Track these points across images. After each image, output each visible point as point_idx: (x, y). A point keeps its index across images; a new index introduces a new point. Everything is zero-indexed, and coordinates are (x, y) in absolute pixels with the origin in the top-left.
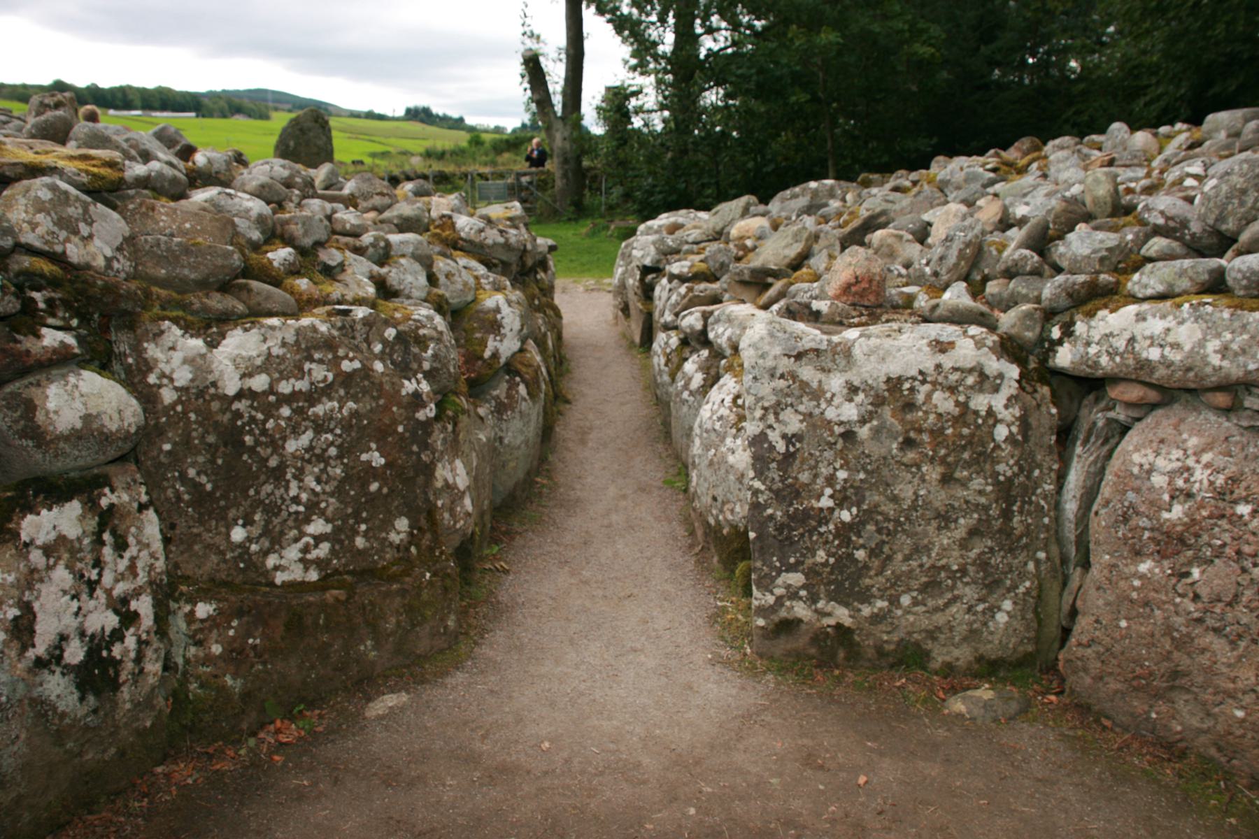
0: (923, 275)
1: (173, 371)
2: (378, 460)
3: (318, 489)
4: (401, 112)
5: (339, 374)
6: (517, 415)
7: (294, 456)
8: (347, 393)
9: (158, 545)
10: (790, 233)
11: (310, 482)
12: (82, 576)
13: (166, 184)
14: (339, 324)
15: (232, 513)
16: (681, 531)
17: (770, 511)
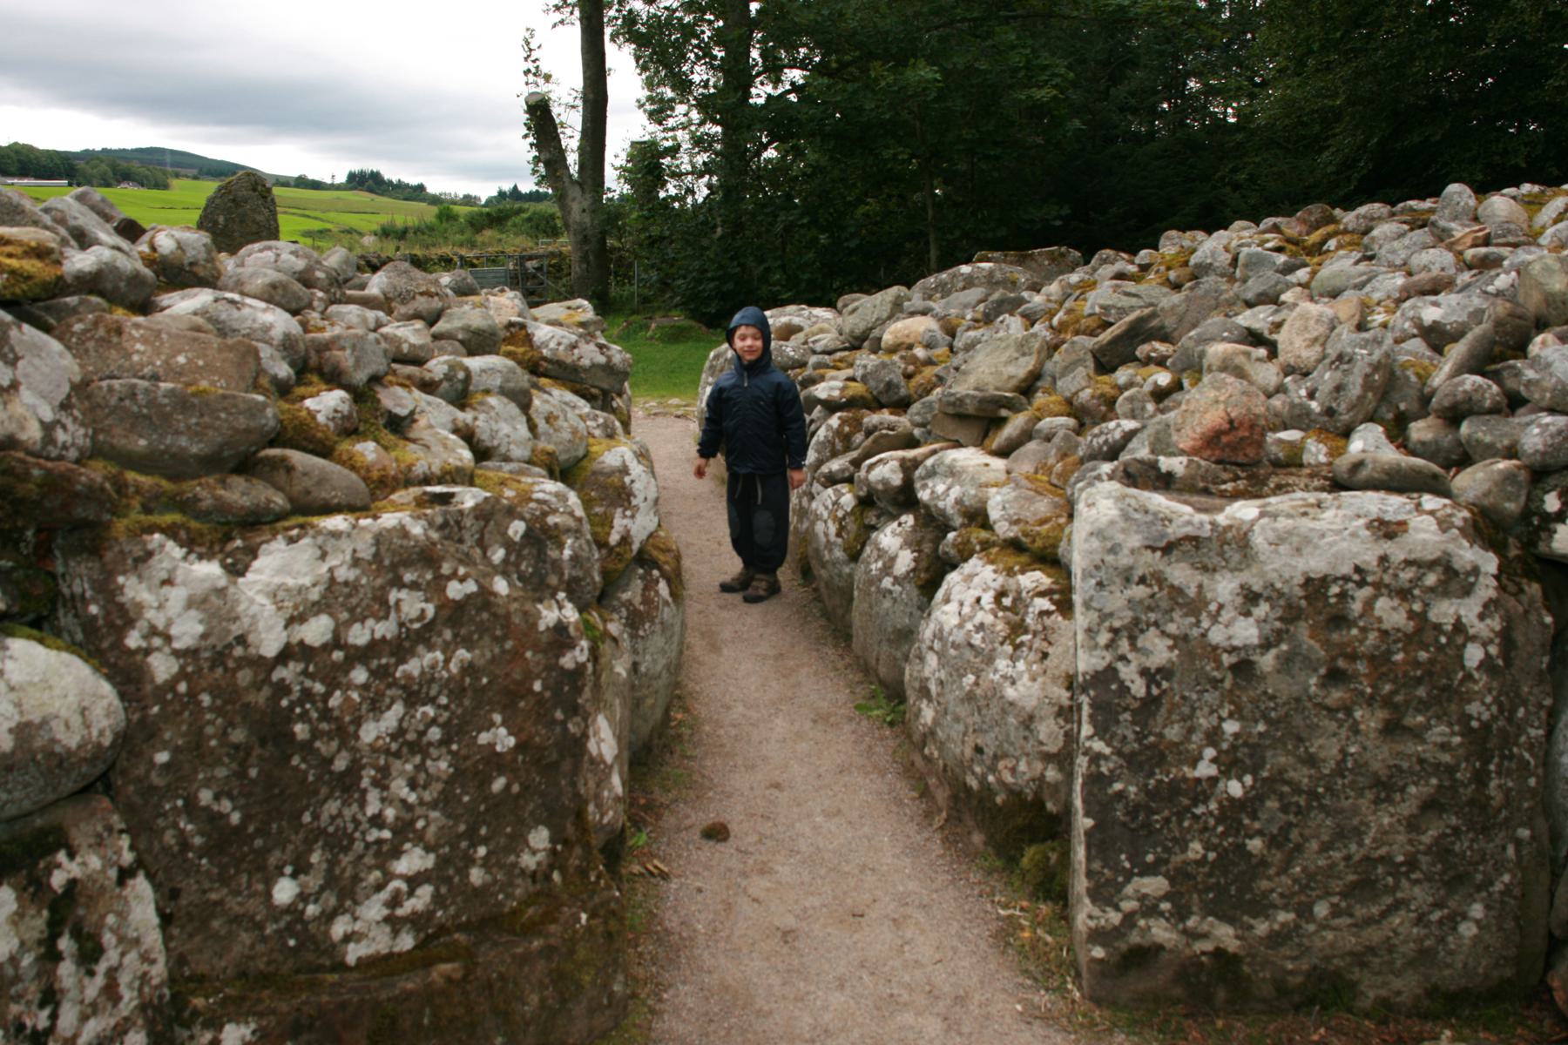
0: (1308, 413)
1: (169, 623)
2: (502, 739)
3: (412, 798)
4: (341, 178)
6: (658, 628)
7: (373, 749)
8: (456, 636)
9: (153, 938)
11: (400, 788)
12: (21, 1027)
13: (122, 284)
14: (439, 520)
15: (274, 858)
16: (906, 792)
17: (1118, 786)
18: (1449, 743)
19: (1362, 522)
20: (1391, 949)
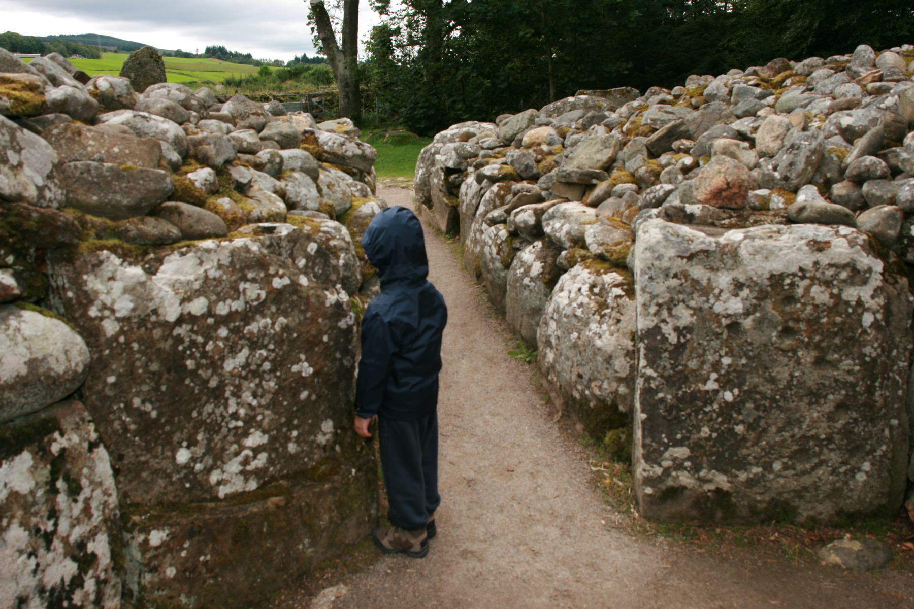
0: (773, 179)
1: (114, 302)
2: (306, 369)
3: (255, 403)
4: (202, 51)
5: (271, 291)
7: (232, 374)
8: (278, 309)
9: (109, 482)
11: (247, 397)
12: (38, 530)
13: (79, 108)
14: (267, 242)
15: (177, 437)
16: (537, 401)
17: (661, 395)
18: (852, 370)
19: (804, 241)
20: (817, 488)
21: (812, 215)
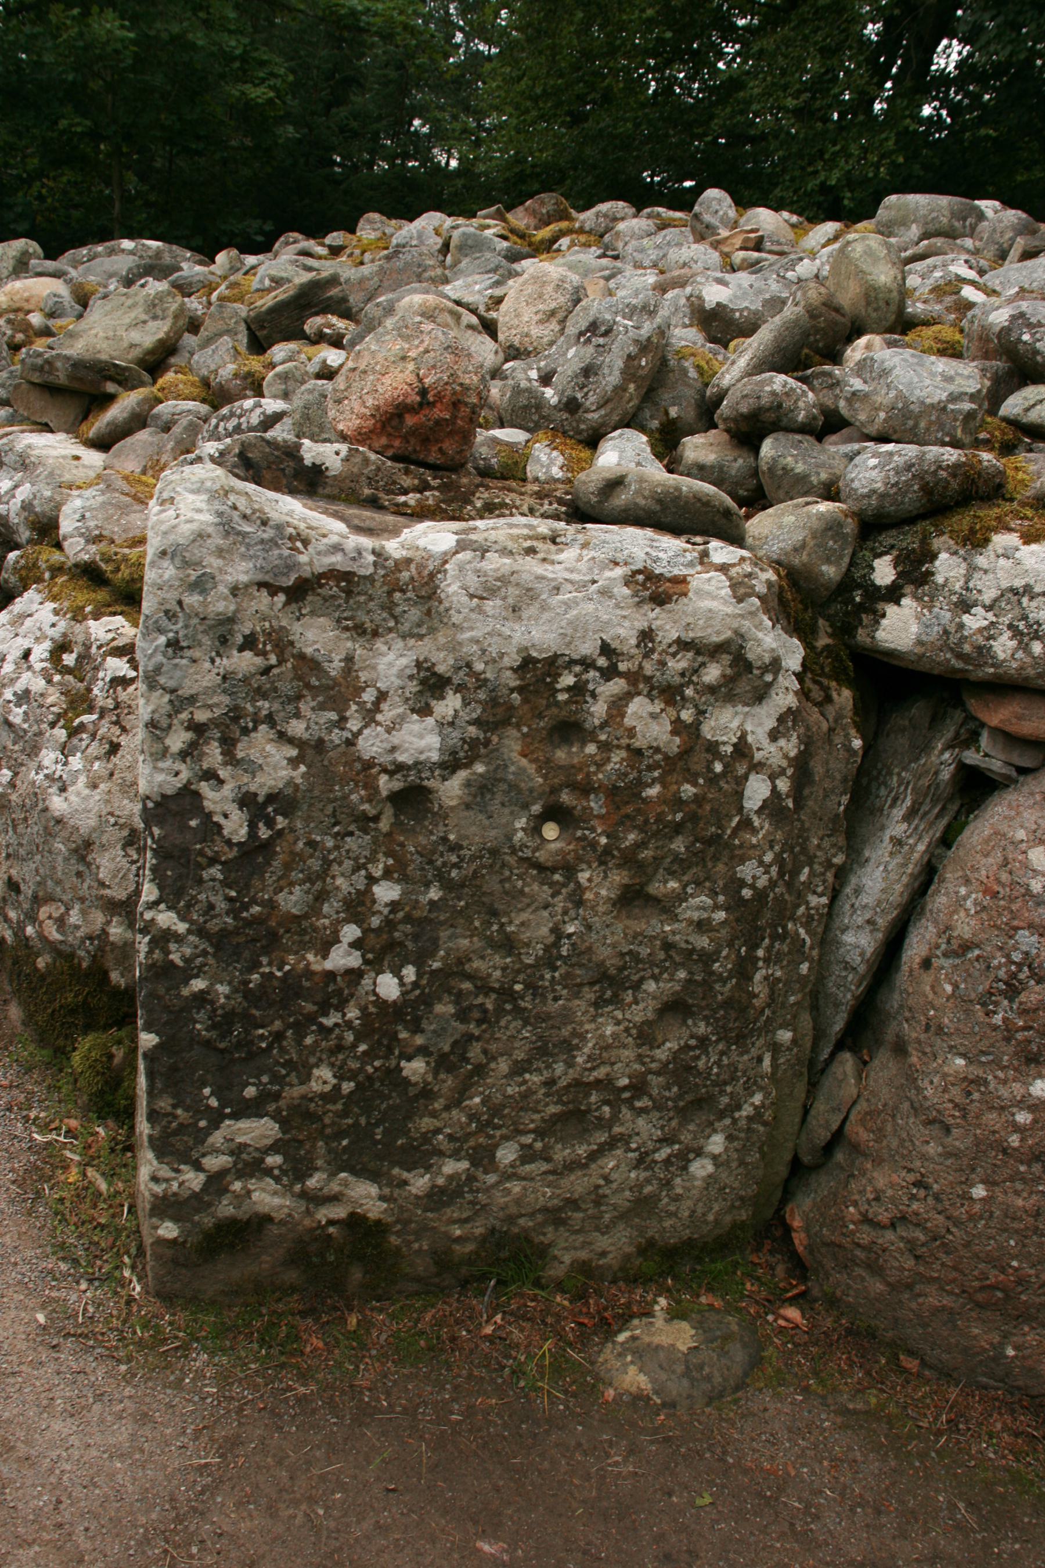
0: (539, 404)
10: (140, 299)
17: (198, 984)
18: (709, 920)
19: (619, 572)
20: (599, 1200)
21: (642, 502)
